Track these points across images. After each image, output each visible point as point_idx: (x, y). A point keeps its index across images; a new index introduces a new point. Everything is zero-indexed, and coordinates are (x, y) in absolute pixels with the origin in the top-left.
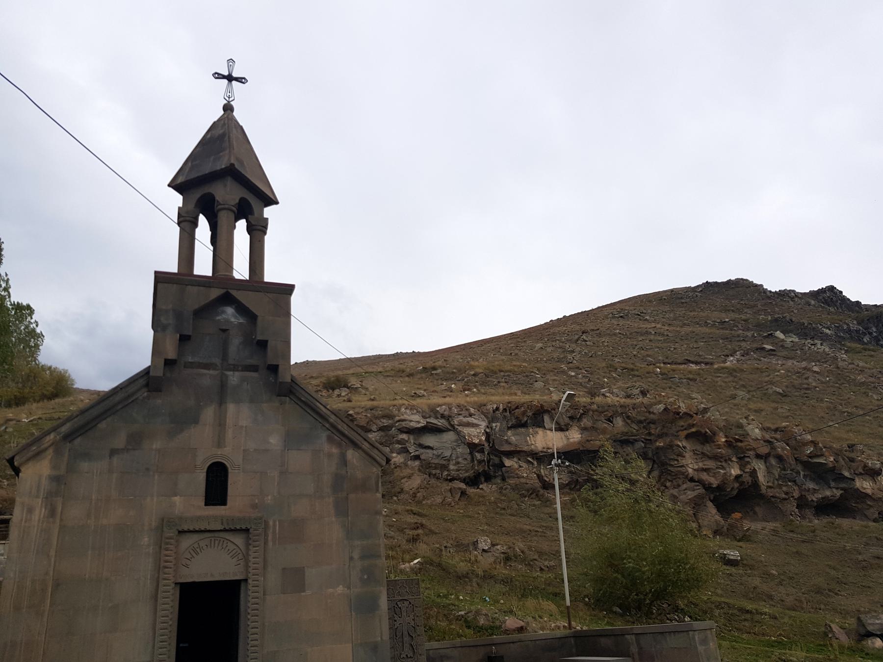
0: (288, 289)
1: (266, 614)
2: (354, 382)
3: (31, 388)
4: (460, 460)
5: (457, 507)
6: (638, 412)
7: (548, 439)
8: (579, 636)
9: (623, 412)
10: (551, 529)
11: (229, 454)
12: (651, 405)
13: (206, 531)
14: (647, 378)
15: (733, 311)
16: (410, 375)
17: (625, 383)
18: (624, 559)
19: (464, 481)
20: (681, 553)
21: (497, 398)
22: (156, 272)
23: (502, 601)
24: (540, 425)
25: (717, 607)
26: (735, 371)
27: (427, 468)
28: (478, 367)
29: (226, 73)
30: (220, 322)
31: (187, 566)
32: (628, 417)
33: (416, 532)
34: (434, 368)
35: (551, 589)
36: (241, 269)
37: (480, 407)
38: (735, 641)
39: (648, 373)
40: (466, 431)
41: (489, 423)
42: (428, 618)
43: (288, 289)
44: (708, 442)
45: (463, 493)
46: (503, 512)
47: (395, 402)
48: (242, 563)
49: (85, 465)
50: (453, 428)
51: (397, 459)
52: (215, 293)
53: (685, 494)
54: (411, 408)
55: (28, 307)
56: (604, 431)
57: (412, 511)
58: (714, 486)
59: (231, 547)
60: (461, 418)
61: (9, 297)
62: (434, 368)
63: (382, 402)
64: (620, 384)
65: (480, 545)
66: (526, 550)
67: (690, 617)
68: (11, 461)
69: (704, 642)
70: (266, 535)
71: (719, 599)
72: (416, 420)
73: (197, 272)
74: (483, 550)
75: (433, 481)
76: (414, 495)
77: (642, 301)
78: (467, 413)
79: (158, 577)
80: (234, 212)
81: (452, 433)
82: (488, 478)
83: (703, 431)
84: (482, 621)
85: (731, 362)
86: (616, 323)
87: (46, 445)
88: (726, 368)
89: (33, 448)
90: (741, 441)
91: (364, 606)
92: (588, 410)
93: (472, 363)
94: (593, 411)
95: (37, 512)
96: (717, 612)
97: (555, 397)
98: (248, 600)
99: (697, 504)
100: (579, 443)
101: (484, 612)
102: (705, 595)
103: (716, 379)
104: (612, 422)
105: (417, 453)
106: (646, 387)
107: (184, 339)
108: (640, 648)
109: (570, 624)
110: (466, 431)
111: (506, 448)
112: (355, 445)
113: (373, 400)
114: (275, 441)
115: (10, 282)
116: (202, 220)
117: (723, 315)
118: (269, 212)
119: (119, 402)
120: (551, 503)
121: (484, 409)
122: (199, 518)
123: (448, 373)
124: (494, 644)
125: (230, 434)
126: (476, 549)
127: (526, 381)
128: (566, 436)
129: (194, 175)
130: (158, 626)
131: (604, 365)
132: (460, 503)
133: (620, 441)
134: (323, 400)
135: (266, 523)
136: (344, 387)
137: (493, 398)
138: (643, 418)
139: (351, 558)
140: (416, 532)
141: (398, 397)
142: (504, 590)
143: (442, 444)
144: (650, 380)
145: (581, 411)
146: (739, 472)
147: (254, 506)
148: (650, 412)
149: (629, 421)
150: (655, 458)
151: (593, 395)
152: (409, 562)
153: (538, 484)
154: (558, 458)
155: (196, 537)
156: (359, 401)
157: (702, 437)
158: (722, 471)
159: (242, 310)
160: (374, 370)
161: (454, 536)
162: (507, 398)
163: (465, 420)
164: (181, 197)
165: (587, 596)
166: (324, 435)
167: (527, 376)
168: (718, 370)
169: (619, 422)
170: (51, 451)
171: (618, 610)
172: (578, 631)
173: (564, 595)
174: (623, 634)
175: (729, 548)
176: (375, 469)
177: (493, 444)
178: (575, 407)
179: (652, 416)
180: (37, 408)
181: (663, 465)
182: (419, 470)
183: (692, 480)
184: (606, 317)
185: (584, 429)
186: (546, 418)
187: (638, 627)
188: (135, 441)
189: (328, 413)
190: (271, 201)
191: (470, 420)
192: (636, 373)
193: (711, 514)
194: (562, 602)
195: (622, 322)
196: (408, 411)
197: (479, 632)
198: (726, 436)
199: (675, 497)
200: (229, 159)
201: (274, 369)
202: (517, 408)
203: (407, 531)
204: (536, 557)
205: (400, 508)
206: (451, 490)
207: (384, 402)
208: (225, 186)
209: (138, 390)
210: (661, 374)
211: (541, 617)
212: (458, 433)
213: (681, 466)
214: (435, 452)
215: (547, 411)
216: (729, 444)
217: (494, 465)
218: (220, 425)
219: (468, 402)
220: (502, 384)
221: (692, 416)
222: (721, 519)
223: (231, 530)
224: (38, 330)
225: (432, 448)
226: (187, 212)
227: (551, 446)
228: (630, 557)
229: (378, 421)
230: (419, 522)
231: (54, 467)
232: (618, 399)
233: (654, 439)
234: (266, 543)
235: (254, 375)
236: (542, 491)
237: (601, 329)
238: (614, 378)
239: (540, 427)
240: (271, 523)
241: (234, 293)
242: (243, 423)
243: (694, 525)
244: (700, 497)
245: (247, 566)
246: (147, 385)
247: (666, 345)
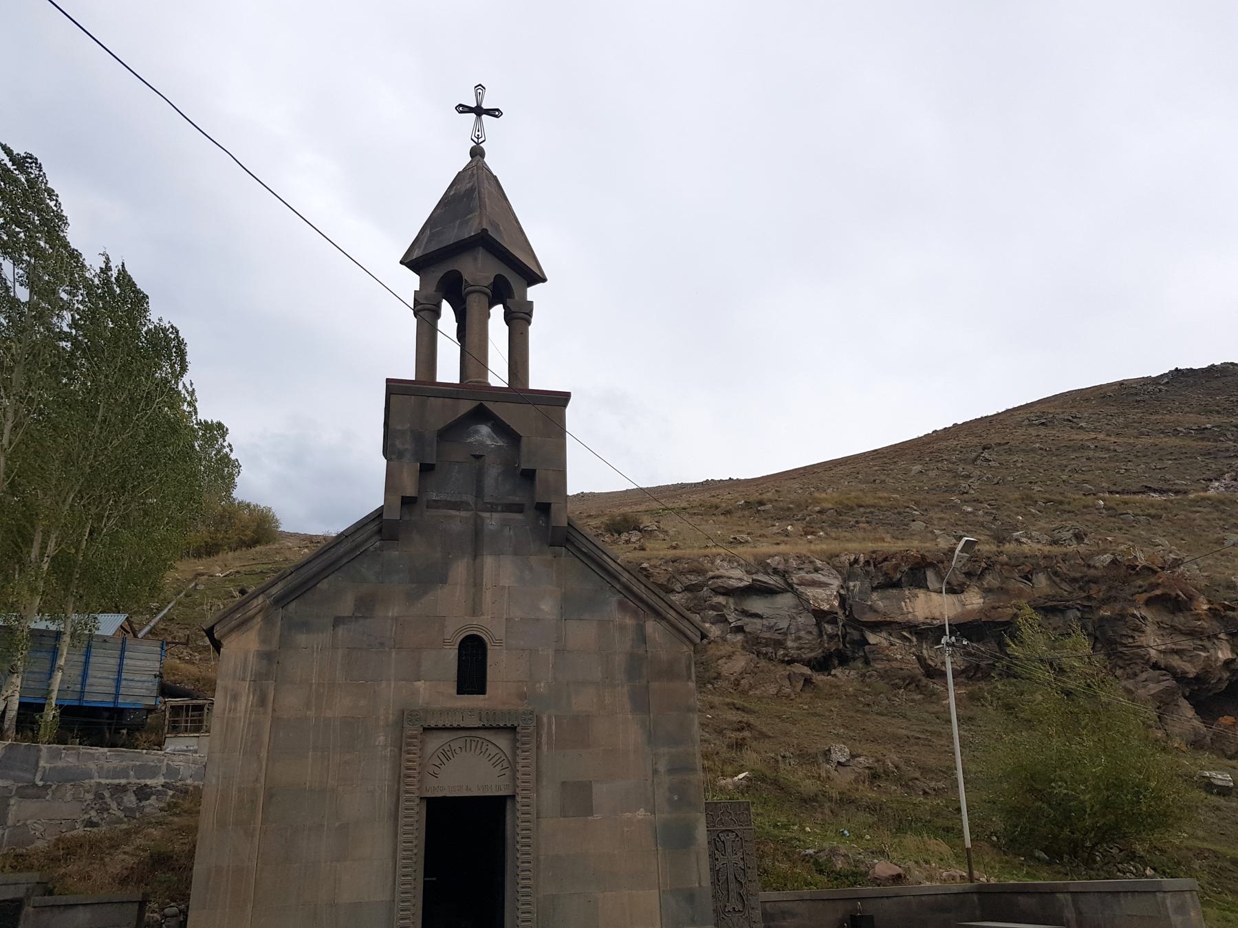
0: (562, 399)
1: (542, 845)
2: (647, 522)
3: (226, 532)
4: (802, 633)
5: (798, 700)
6: (1071, 566)
7: (931, 605)
8: (984, 892)
9: (1048, 565)
10: (940, 734)
11: (488, 625)
12: (1092, 555)
13: (459, 729)
14: (1082, 514)
15: (1218, 412)
16: (727, 513)
17: (1049, 522)
18: (1053, 781)
19: (808, 663)
20: (1140, 773)
21: (856, 546)
22: (388, 380)
23: (868, 837)
24: (922, 584)
25: (1197, 856)
26: (1223, 503)
27: (754, 644)
28: (826, 500)
29: (474, 105)
30: (472, 446)
31: (435, 775)
32: (1056, 573)
33: (740, 735)
34: (761, 503)
35: (940, 822)
36: (498, 374)
37: (831, 558)
38: (1229, 909)
39: (1085, 507)
40: (810, 592)
41: (845, 581)
42: (762, 857)
43: (562, 399)
44: (1181, 611)
45: (808, 681)
46: (866, 709)
47: (707, 551)
48: (507, 772)
49: (302, 639)
50: (790, 588)
51: (714, 631)
52: (466, 406)
53: (1145, 687)
54: (731, 559)
55: (220, 426)
56: (1020, 594)
57: (734, 704)
58: (1191, 676)
59: (493, 750)
60: (802, 574)
61: (196, 413)
62: (761, 503)
63: (688, 551)
64: (1042, 524)
65: (833, 756)
66: (902, 765)
67: (1154, 869)
68: (210, 632)
69: (1181, 909)
70: (539, 735)
71: (1199, 844)
72: (737, 577)
73: (440, 378)
74: (839, 763)
75: (763, 663)
76: (737, 683)
77: (1074, 400)
78: (811, 567)
79: (399, 789)
80: (486, 294)
81: (789, 595)
82: (844, 660)
83: (1173, 594)
84: (839, 864)
85: (1216, 490)
86: (1034, 433)
87: (252, 612)
88: (1209, 498)
89: (236, 617)
90: (1233, 609)
91: (676, 839)
92: (994, 563)
93: (817, 495)
94: (1002, 565)
95: (244, 699)
96: (1196, 864)
97: (943, 544)
98: (516, 824)
99: (1164, 703)
100: (981, 611)
101: (843, 851)
102: (1179, 838)
103: (1193, 516)
104: (1030, 580)
105: (739, 623)
106: (1083, 528)
107: (426, 469)
108: (1079, 913)
109: (971, 874)
110: (810, 592)
111: (870, 617)
112: (658, 615)
113: (675, 548)
114: (548, 607)
115: (196, 394)
116: (446, 309)
117: (1203, 419)
118: (534, 293)
119: (341, 558)
120: (936, 697)
121: (836, 561)
122: (449, 712)
123: (782, 509)
124: (859, 899)
125: (488, 597)
126: (828, 761)
127: (899, 521)
128: (961, 601)
129: (433, 247)
130: (399, 856)
131: (1017, 495)
132: (804, 695)
133: (1043, 608)
134: (608, 548)
135: (539, 719)
136: (635, 529)
137: (851, 546)
138: (1078, 575)
139: (655, 772)
140: (740, 735)
141: (711, 544)
142: (871, 821)
143: (775, 611)
144: (1088, 517)
145: (983, 565)
146: (1230, 655)
147: (522, 696)
148: (1089, 566)
149: (1057, 580)
150: (1098, 633)
151: (1000, 540)
152: (732, 777)
153: (919, 671)
154: (951, 634)
155: (446, 737)
156: (654, 549)
157: (1173, 603)
158: (1203, 654)
159: (501, 428)
160: (676, 505)
161: (796, 741)
162: (870, 546)
163: (808, 577)
164: (418, 277)
165: (995, 833)
166: (614, 599)
167: (899, 513)
168: (1195, 502)
169: (1041, 581)
170: (259, 618)
171: (1043, 855)
172: (982, 885)
173: (961, 831)
174: (1052, 892)
175: (1214, 769)
176: (685, 648)
177: (851, 612)
178: (974, 559)
179: (1092, 571)
180: (234, 559)
181: (1111, 642)
182: (744, 648)
183: (1156, 666)
184: (1020, 425)
185: (987, 591)
186: (930, 575)
187: (1076, 883)
188: (366, 606)
189: (619, 568)
190: (536, 277)
191: (816, 576)
192: (1067, 507)
193: (1186, 717)
194: (958, 841)
195: (1043, 431)
196: (725, 564)
197: (836, 879)
198: (1209, 602)
199: (1129, 691)
200: (480, 223)
201: (544, 509)
202: (885, 560)
203: (728, 733)
204: (917, 775)
205: (717, 700)
206: (789, 677)
207: (691, 551)
208: (476, 260)
209: (370, 537)
210: (1106, 508)
211: (927, 862)
212: (799, 596)
213: (1139, 647)
214: (765, 622)
215: (931, 565)
216: (1213, 613)
217: (853, 642)
218: (475, 585)
219: (812, 552)
220: (861, 525)
221: (1155, 572)
222: (1201, 726)
223: (491, 728)
224: (233, 456)
225: (761, 617)
226: (426, 298)
227: (937, 615)
228: (1062, 779)
229: (683, 579)
230: (745, 720)
231: (264, 641)
232: (1039, 546)
233: (1099, 603)
234: (538, 747)
235: (518, 516)
236: (924, 681)
237: (1012, 443)
238: (1033, 515)
239: (920, 587)
240: (545, 720)
241: (490, 406)
242: (506, 582)
243: (1159, 734)
244: (1166, 691)
245: (514, 778)
246: (380, 531)
247: (1112, 465)
